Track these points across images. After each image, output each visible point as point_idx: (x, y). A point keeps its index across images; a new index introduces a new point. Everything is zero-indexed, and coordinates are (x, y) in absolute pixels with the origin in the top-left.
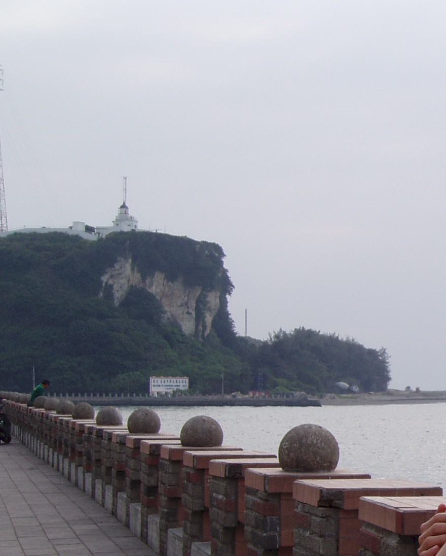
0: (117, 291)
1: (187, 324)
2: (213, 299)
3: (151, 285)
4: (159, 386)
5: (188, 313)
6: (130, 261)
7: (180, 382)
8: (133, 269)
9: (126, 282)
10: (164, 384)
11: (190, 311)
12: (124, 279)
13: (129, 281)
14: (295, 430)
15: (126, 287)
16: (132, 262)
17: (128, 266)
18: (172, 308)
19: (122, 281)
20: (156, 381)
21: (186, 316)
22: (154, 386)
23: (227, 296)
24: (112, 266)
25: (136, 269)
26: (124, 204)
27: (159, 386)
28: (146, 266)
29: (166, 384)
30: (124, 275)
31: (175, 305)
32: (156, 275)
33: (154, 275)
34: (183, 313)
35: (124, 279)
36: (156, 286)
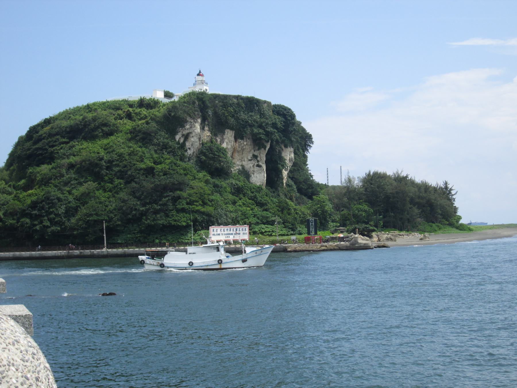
0: (189, 149)
1: (258, 176)
2: (289, 155)
3: (222, 141)
4: (219, 234)
5: (258, 166)
6: (199, 120)
7: (239, 230)
8: (203, 129)
9: (197, 140)
10: (224, 233)
11: (260, 163)
12: (195, 138)
13: (200, 139)
14: (376, 174)
15: (197, 145)
16: (202, 121)
17: (198, 126)
18: (244, 163)
19: (192, 139)
20: (215, 231)
21: (256, 169)
22: (214, 235)
23: (461, 222)
24: (183, 126)
25: (206, 128)
26: (200, 72)
27: (219, 234)
28: (219, 126)
29: (226, 232)
30: (194, 134)
31: (246, 159)
32: (226, 132)
33: (224, 133)
34: (253, 166)
35: (195, 138)
36: (227, 143)
